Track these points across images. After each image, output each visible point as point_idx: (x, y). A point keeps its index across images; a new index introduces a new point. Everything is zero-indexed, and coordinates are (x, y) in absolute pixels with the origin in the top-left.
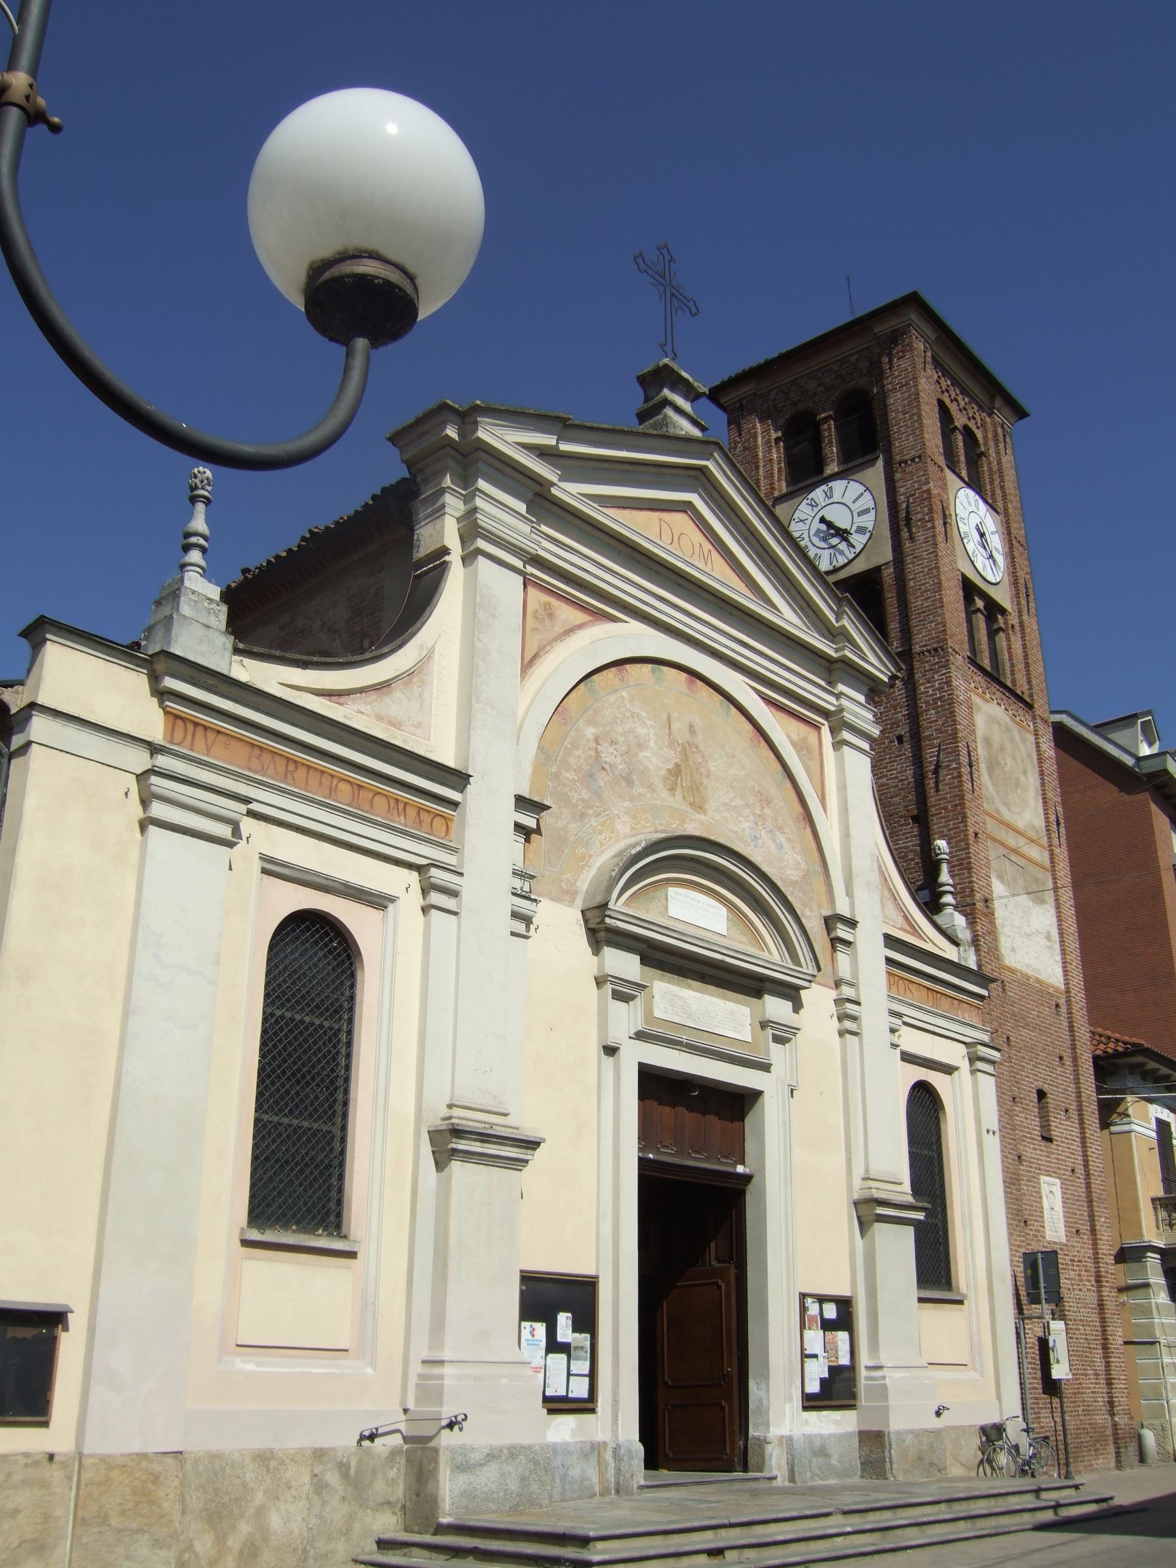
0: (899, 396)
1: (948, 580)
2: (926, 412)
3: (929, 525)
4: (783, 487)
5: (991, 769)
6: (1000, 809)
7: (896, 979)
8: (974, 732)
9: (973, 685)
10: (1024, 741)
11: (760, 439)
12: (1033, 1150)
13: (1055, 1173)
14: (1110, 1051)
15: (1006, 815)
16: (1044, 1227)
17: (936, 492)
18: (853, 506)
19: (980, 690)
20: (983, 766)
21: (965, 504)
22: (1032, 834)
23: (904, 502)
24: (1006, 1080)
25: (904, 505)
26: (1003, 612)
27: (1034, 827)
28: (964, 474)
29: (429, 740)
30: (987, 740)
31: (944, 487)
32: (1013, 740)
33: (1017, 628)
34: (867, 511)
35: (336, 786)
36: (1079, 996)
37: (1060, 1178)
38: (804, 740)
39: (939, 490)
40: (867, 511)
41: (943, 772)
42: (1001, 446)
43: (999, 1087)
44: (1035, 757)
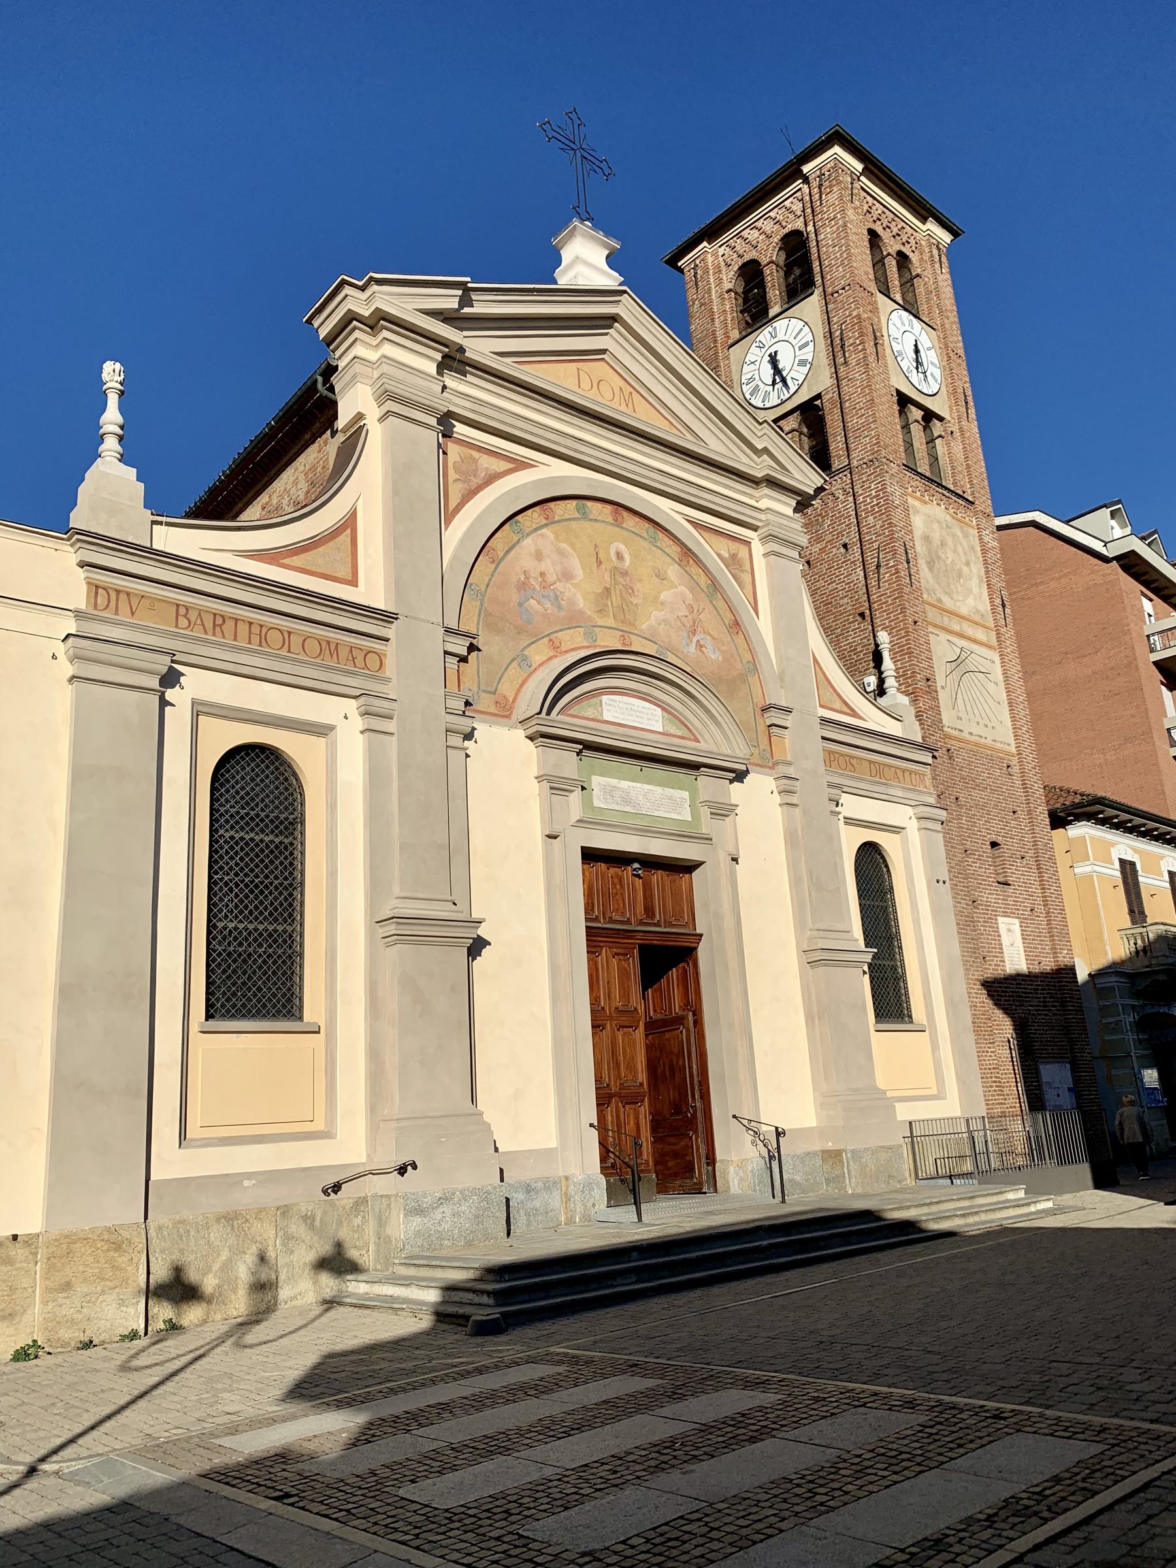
0: (829, 230)
1: (880, 396)
2: (853, 242)
3: (860, 347)
4: (735, 334)
5: (931, 565)
6: (942, 598)
7: (837, 756)
8: (911, 532)
9: (910, 489)
10: (966, 536)
11: (713, 293)
12: (990, 895)
13: (1014, 913)
14: (1067, 803)
15: (948, 603)
16: (1004, 962)
17: (866, 316)
18: (794, 343)
19: (918, 494)
20: (922, 564)
21: (898, 323)
22: (977, 618)
23: (837, 330)
24: (956, 836)
25: (838, 333)
26: (941, 419)
27: (978, 611)
28: (898, 298)
29: (354, 582)
30: (927, 539)
31: (875, 310)
32: (954, 536)
33: (957, 434)
34: (806, 344)
35: (266, 633)
36: (1030, 758)
37: (1019, 918)
38: (734, 556)
39: (870, 314)
40: (806, 344)
41: (882, 570)
42: (937, 266)
43: (948, 843)
44: (978, 549)
